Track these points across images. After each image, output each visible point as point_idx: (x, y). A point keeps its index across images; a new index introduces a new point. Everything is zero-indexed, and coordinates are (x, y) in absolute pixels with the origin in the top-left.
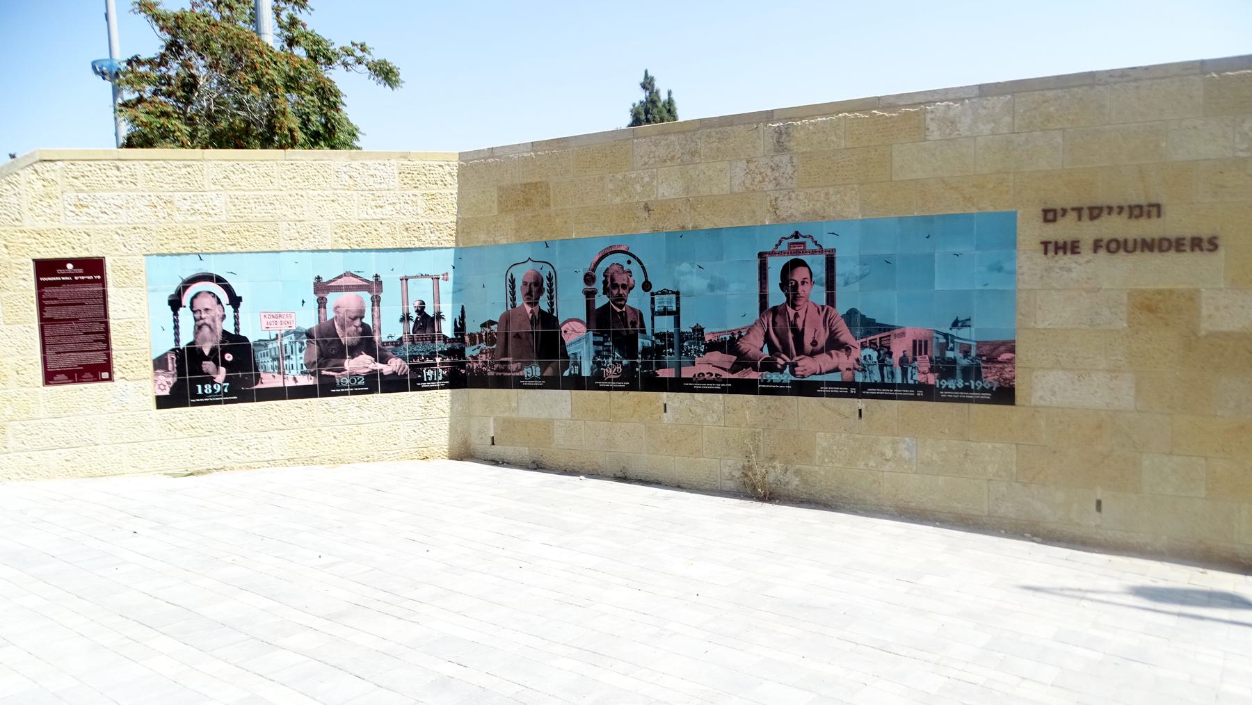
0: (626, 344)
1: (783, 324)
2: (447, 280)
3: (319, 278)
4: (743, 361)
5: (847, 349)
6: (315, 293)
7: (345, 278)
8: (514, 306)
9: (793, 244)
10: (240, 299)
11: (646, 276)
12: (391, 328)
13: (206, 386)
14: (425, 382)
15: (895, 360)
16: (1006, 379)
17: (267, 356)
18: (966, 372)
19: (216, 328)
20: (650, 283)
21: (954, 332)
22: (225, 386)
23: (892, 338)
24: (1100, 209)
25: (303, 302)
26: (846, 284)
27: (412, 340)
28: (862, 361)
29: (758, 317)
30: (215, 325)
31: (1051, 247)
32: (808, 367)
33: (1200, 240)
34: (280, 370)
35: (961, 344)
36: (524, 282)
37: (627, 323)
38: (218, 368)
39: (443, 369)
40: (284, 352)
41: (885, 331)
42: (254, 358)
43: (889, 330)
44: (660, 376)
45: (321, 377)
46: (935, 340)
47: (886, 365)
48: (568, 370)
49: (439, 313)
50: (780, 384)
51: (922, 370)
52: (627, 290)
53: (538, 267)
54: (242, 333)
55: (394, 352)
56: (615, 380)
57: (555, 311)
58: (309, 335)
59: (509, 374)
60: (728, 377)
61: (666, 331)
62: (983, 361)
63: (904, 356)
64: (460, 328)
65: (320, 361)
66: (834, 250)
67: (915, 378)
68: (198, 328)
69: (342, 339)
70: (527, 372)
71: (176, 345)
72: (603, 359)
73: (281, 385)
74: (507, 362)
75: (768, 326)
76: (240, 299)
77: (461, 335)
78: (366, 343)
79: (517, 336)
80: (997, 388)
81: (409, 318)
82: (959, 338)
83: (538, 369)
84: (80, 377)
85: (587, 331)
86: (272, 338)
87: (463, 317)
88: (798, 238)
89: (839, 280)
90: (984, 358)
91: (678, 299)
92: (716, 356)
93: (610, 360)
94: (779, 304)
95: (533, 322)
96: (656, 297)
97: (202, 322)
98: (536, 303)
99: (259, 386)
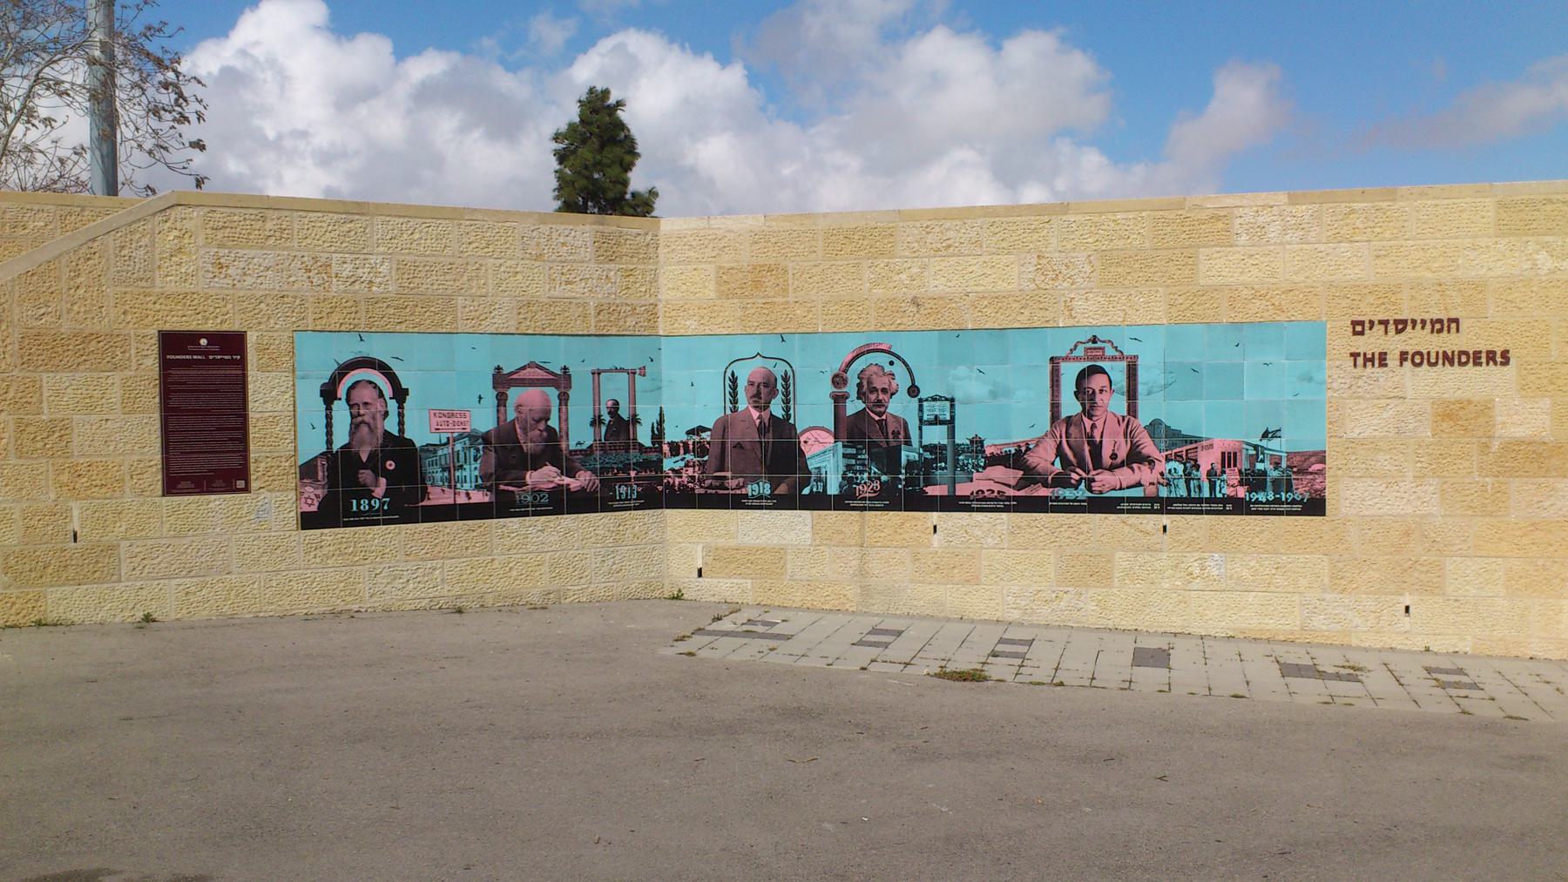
0: (889, 458)
3: (499, 368)
4: (1031, 476)
5: (1151, 462)
6: (494, 388)
7: (528, 370)
8: (734, 410)
9: (1090, 349)
10: (406, 392)
11: (913, 380)
12: (580, 434)
13: (362, 502)
15: (1202, 473)
16: (1316, 491)
17: (436, 465)
19: (376, 428)
20: (917, 388)
21: (1264, 443)
22: (385, 502)
23: (1199, 449)
25: (480, 398)
28: (1167, 475)
29: (1049, 429)
30: (375, 424)
31: (1360, 360)
32: (1106, 482)
33: (1494, 353)
34: (452, 484)
35: (1271, 455)
36: (749, 381)
37: (887, 434)
38: (377, 480)
40: (456, 460)
41: (1191, 443)
42: (421, 467)
43: (1196, 442)
44: (929, 494)
45: (499, 493)
46: (1244, 451)
47: (1193, 479)
48: (809, 487)
49: (635, 415)
50: (1075, 500)
51: (1231, 483)
52: (889, 395)
53: (770, 364)
54: (407, 436)
58: (486, 438)
59: (726, 492)
61: (937, 443)
62: (1294, 473)
64: (658, 434)
65: (498, 472)
66: (1136, 357)
67: (1223, 491)
68: (355, 428)
69: (524, 446)
70: (751, 489)
71: (328, 448)
72: (856, 474)
74: (725, 478)
75: (1061, 437)
76: (406, 392)
78: (552, 450)
79: (738, 446)
80: (1308, 499)
81: (601, 422)
83: (768, 486)
85: (835, 442)
87: (661, 422)
88: (1096, 342)
90: (1295, 469)
91: (952, 406)
92: (998, 472)
93: (866, 475)
95: (762, 429)
96: (925, 404)
97: (360, 419)
98: (766, 407)
99: (425, 503)
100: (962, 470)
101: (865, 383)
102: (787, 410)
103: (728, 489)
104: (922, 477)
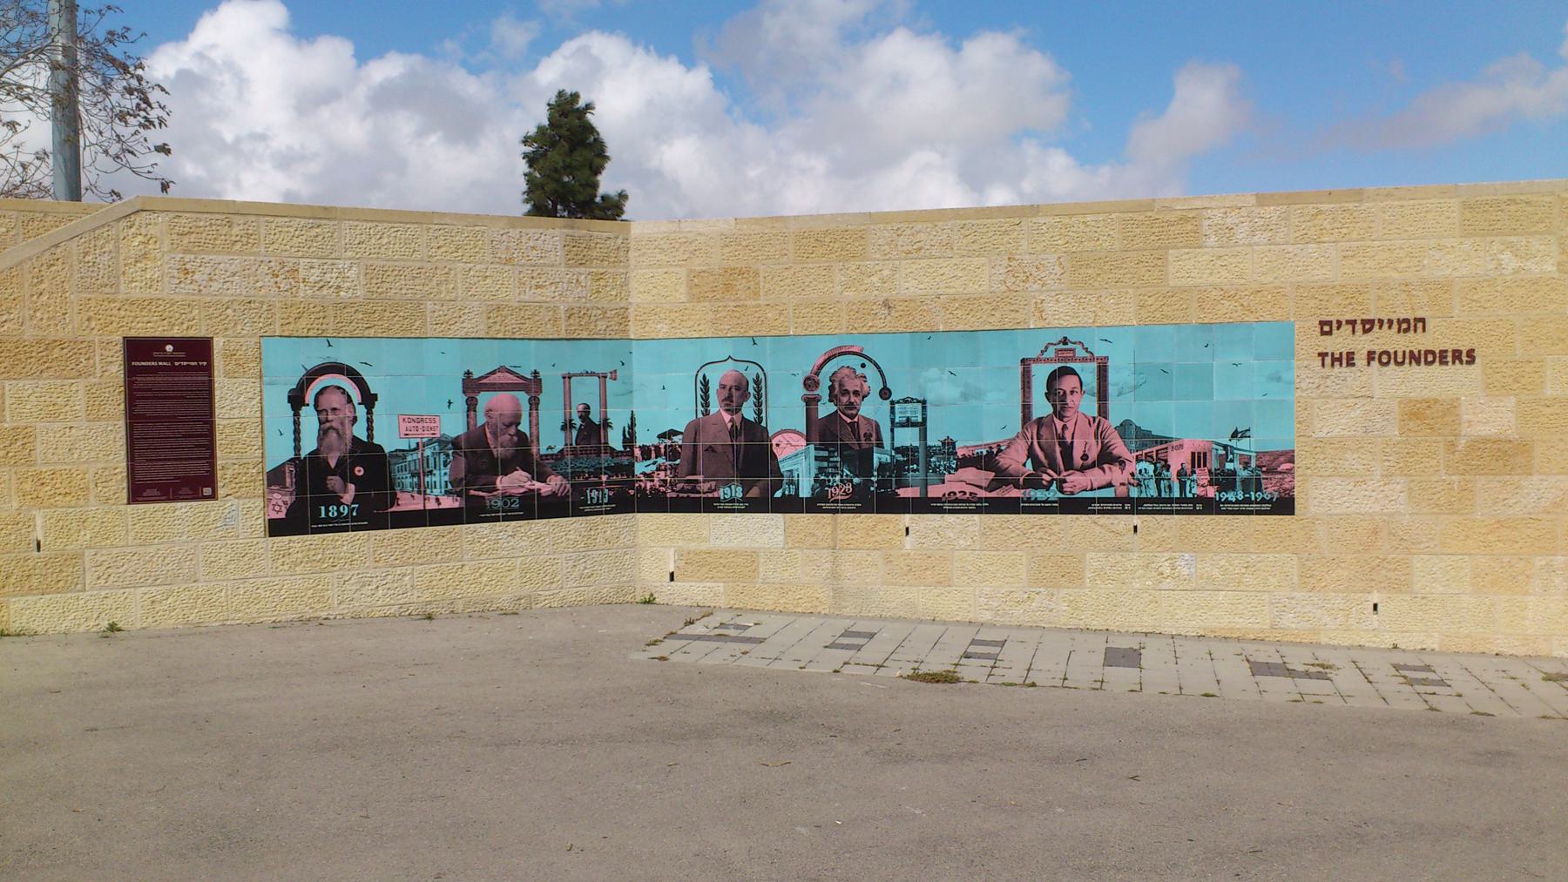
0: (860, 460)
1: (1049, 437)
2: (615, 379)
4: (1003, 478)
5: (1121, 462)
6: (464, 392)
7: (499, 374)
8: (706, 413)
9: (1061, 350)
10: (375, 397)
11: (884, 382)
12: (551, 439)
14: (589, 505)
15: (1173, 473)
16: (1285, 490)
18: (1246, 483)
19: (345, 434)
21: (1233, 443)
22: (354, 508)
23: (1169, 450)
24: (1372, 322)
25: (450, 403)
26: (1120, 394)
27: (574, 452)
28: (1137, 475)
29: (1020, 430)
31: (1328, 360)
32: (1078, 482)
35: (1240, 455)
36: (721, 385)
38: (346, 486)
39: (610, 489)
40: (425, 465)
41: (1161, 444)
42: (390, 473)
43: (1166, 442)
45: (469, 498)
47: (1163, 479)
49: (606, 420)
50: (1046, 501)
51: (1201, 483)
52: (861, 397)
53: (741, 367)
54: (375, 441)
55: (554, 468)
56: (843, 501)
57: (764, 420)
58: (455, 443)
60: (984, 496)
62: (1263, 472)
63: (1182, 469)
64: (629, 439)
66: (1106, 358)
68: (323, 434)
70: (724, 492)
72: (828, 477)
73: (420, 507)
74: (697, 481)
76: (375, 397)
77: (630, 447)
78: (523, 455)
79: (710, 449)
81: (572, 426)
82: (1239, 450)
83: (740, 489)
84: (175, 493)
85: (807, 445)
86: (412, 447)
87: (632, 426)
88: (1067, 344)
89: (1112, 390)
90: (1264, 469)
91: (924, 408)
92: (970, 474)
93: (838, 478)
94: (1045, 416)
95: (734, 433)
96: (897, 406)
97: (328, 425)
98: (738, 410)
99: (394, 509)
100: (935, 471)
101: (837, 386)
102: (759, 413)
103: (700, 493)
104: (894, 479)
